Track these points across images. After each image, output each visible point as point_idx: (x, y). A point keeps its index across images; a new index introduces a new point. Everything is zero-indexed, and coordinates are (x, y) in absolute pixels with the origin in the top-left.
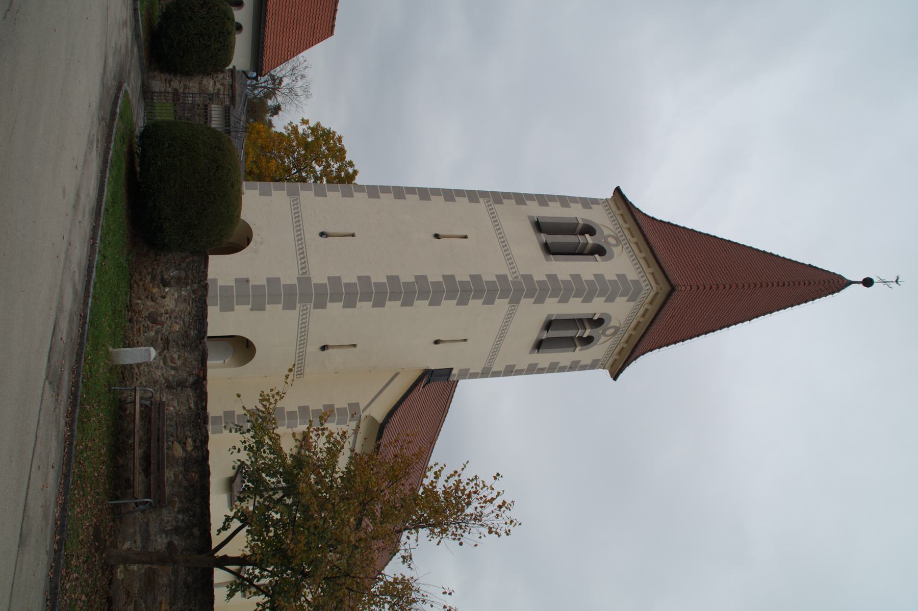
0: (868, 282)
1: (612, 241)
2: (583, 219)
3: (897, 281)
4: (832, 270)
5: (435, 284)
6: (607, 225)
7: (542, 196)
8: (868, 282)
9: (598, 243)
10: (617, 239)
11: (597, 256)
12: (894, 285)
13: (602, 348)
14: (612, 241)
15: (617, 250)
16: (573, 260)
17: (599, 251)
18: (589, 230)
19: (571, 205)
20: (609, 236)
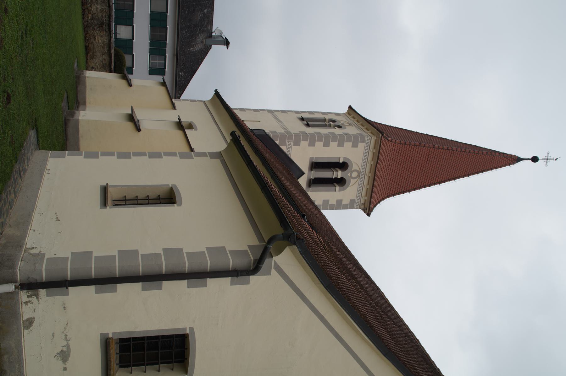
0: (535, 159)
8: (535, 159)
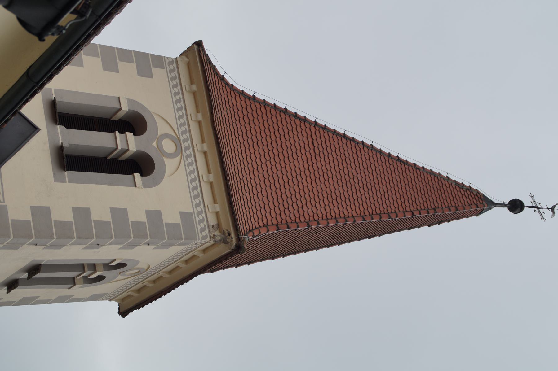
0: (516, 206)
1: (168, 146)
2: (130, 101)
3: (553, 209)
4: (22, 149)
5: (137, 225)
6: (166, 108)
7: (145, 55)
8: (516, 206)
9: (143, 149)
10: (177, 142)
11: (137, 175)
12: (548, 213)
13: (117, 282)
14: (168, 146)
15: (170, 164)
16: (111, 184)
17: (139, 166)
18: (134, 123)
19: (121, 64)
20: (166, 136)
